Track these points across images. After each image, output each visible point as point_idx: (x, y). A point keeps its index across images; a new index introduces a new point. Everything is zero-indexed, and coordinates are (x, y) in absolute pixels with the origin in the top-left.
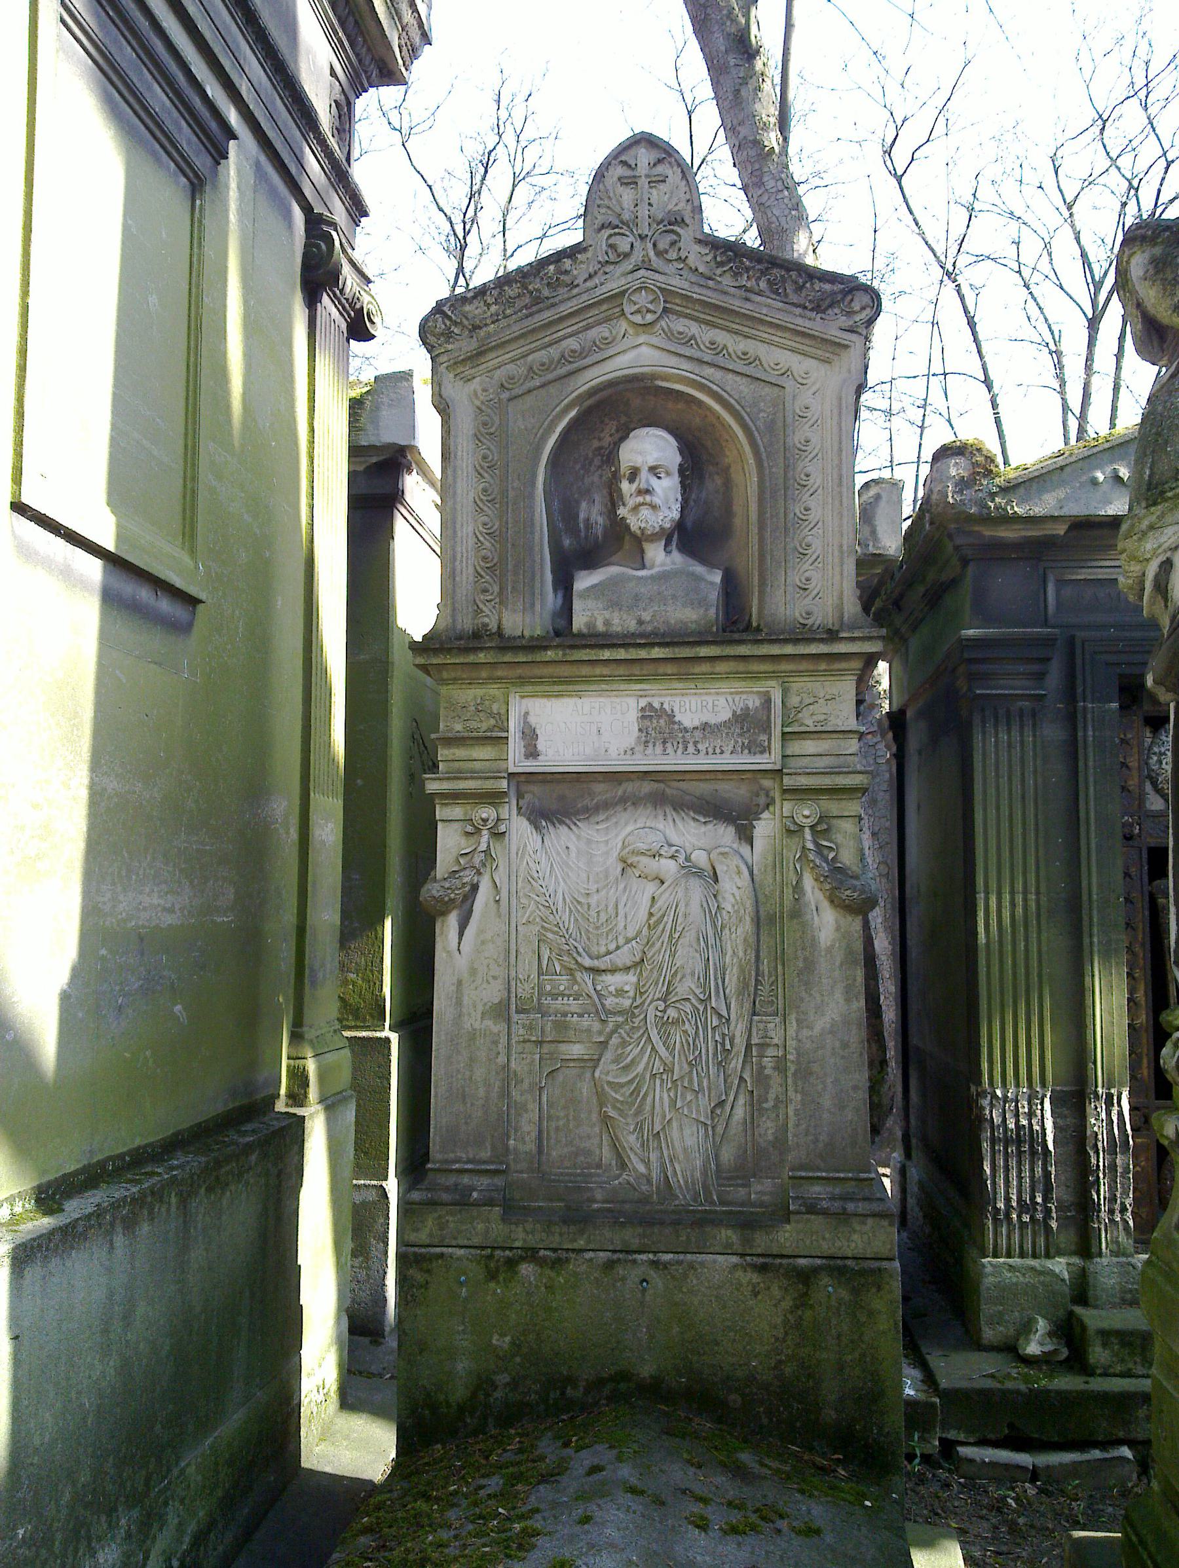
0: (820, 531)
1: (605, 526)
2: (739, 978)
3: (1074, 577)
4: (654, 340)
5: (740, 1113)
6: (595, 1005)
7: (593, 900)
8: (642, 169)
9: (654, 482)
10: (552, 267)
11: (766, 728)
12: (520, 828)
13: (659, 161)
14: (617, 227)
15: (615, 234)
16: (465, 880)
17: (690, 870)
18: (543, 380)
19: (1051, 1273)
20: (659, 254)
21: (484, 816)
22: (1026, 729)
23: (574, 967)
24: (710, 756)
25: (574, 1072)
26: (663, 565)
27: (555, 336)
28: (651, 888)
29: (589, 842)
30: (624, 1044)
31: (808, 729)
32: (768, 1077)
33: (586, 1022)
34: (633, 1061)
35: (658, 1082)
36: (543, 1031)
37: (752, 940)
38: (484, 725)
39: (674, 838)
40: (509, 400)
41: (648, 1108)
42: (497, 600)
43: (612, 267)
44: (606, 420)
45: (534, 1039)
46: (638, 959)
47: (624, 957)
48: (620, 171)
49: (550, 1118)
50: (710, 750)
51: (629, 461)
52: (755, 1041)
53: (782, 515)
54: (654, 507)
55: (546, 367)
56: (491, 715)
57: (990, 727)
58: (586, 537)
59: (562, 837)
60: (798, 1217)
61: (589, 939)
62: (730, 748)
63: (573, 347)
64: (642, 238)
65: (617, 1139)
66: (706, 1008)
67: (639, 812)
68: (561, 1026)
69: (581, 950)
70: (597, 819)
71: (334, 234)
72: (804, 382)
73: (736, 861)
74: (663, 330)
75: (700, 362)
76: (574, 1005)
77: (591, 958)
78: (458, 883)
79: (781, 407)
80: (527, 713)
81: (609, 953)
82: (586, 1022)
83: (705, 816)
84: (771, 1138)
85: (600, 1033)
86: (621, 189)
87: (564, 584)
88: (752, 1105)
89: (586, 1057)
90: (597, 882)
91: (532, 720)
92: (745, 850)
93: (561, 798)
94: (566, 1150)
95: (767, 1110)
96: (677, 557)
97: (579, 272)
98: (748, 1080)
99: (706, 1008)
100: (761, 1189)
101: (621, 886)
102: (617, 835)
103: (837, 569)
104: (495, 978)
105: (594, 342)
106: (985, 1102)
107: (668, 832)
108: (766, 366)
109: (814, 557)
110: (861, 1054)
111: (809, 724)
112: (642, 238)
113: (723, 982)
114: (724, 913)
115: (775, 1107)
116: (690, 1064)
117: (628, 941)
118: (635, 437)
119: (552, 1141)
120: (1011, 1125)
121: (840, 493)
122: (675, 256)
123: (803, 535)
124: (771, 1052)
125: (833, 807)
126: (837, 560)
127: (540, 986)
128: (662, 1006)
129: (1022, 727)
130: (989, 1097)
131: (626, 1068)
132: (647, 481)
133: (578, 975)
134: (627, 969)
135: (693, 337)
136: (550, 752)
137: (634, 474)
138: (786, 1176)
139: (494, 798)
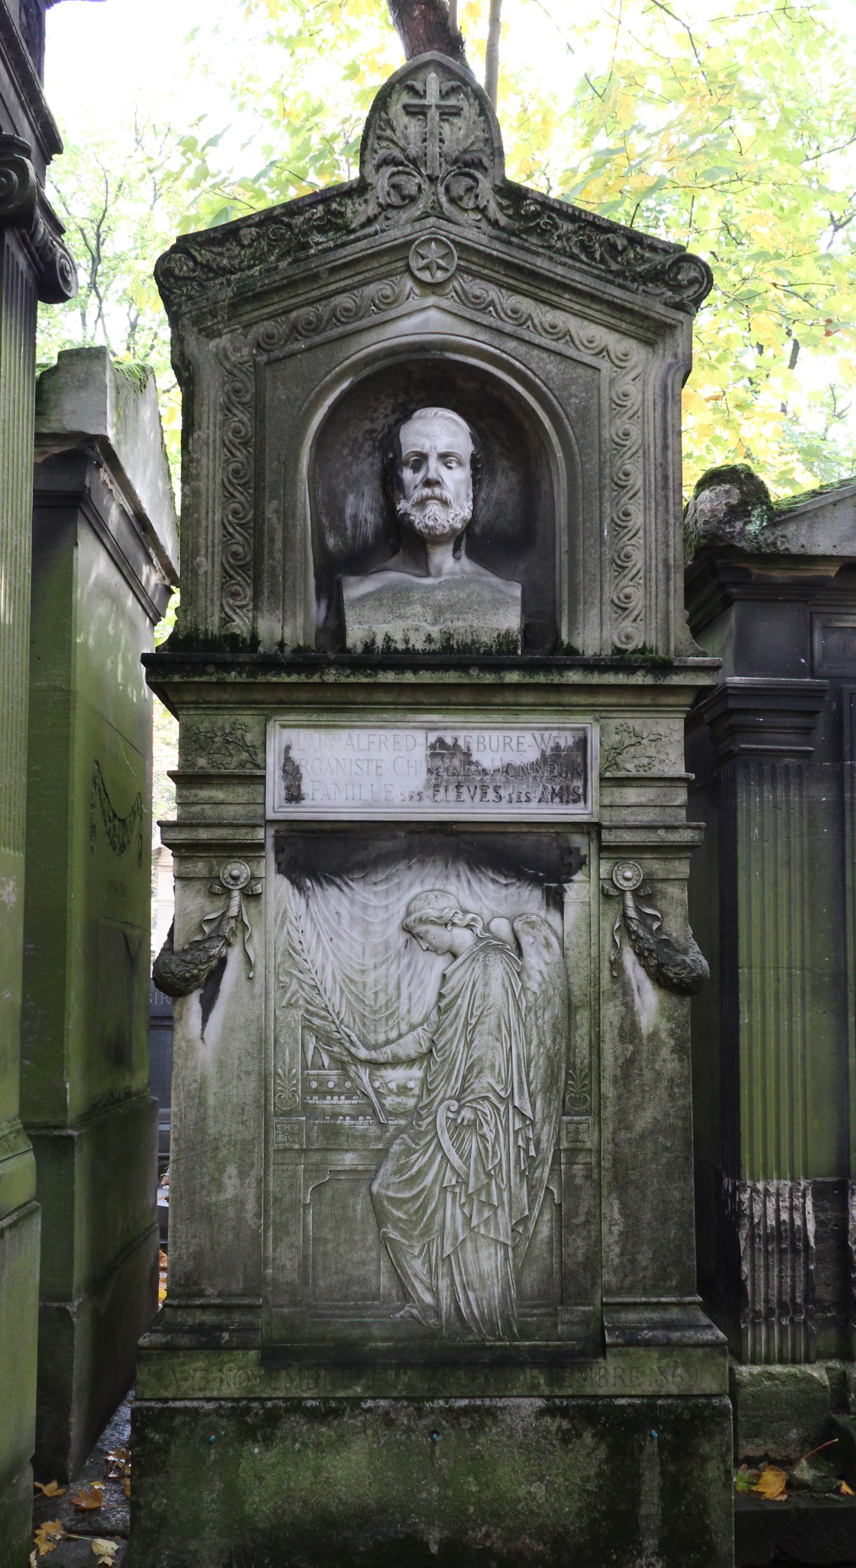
0: (641, 541)
1: (376, 525)
2: (546, 1072)
3: (841, 624)
4: (445, 303)
5: (545, 1231)
6: (371, 1105)
7: (370, 978)
8: (432, 98)
9: (445, 473)
10: (320, 208)
11: (582, 772)
12: (277, 888)
13: (454, 90)
14: (401, 164)
15: (399, 173)
16: (214, 952)
17: (488, 944)
18: (309, 342)
19: (810, 1379)
20: (452, 201)
21: (235, 873)
22: (792, 787)
23: (345, 1059)
24: (524, 804)
25: (347, 1185)
26: (452, 573)
27: (324, 290)
28: (441, 963)
29: (365, 907)
30: (409, 1152)
31: (630, 774)
32: (580, 1188)
33: (362, 1124)
34: (419, 1172)
35: (449, 1197)
36: (308, 1138)
37: (563, 1026)
38: (232, 764)
39: (470, 904)
40: (269, 363)
41: (436, 1228)
42: (251, 607)
43: (395, 212)
44: (382, 397)
45: (297, 1147)
46: (424, 1050)
47: (408, 1046)
48: (406, 98)
49: (316, 1240)
50: (514, 797)
51: (414, 445)
52: (564, 1145)
53: (597, 519)
54: (445, 503)
55: (313, 327)
56: (245, 747)
57: (754, 788)
58: (354, 538)
59: (333, 902)
60: (614, 1350)
61: (364, 1025)
62: (538, 795)
63: (348, 305)
64: (432, 179)
65: (401, 1267)
66: (507, 1108)
67: (426, 871)
68: (332, 1132)
69: (354, 1038)
70: (374, 879)
71: (28, 161)
72: (623, 364)
73: (545, 931)
74: (456, 292)
75: (499, 332)
76: (343, 1103)
77: (368, 1047)
78: (203, 956)
79: (596, 392)
80: (288, 748)
81: (388, 1042)
82: (362, 1124)
83: (506, 876)
84: (580, 1258)
85: (379, 1139)
86: (405, 119)
87: (330, 592)
88: (560, 1220)
89: (360, 1168)
90: (375, 956)
91: (294, 754)
92: (554, 918)
93: (327, 852)
94: (335, 1278)
95: (577, 1226)
96: (467, 565)
97: (357, 211)
98: (555, 1191)
99: (507, 1108)
100: (568, 1323)
101: (404, 962)
102: (399, 900)
103: (662, 587)
104: (248, 1073)
105: (373, 301)
106: (745, 1197)
107: (461, 897)
108: (577, 342)
109: (634, 571)
110: (687, 1159)
111: (631, 768)
112: (432, 179)
113: (528, 1075)
114: (529, 993)
115: (587, 1222)
116: (488, 1175)
117: (413, 1028)
118: (420, 418)
119: (319, 1269)
120: (771, 1221)
121: (666, 498)
122: (471, 205)
123: (621, 544)
124: (582, 1158)
125: (657, 867)
126: (661, 576)
127: (306, 1080)
128: (455, 1106)
129: (787, 786)
130: (749, 1190)
131: (412, 1181)
132: (436, 470)
133: (352, 1069)
134: (410, 1062)
135: (492, 303)
136: (318, 795)
137: (421, 460)
138: (598, 1303)
139: (250, 850)
